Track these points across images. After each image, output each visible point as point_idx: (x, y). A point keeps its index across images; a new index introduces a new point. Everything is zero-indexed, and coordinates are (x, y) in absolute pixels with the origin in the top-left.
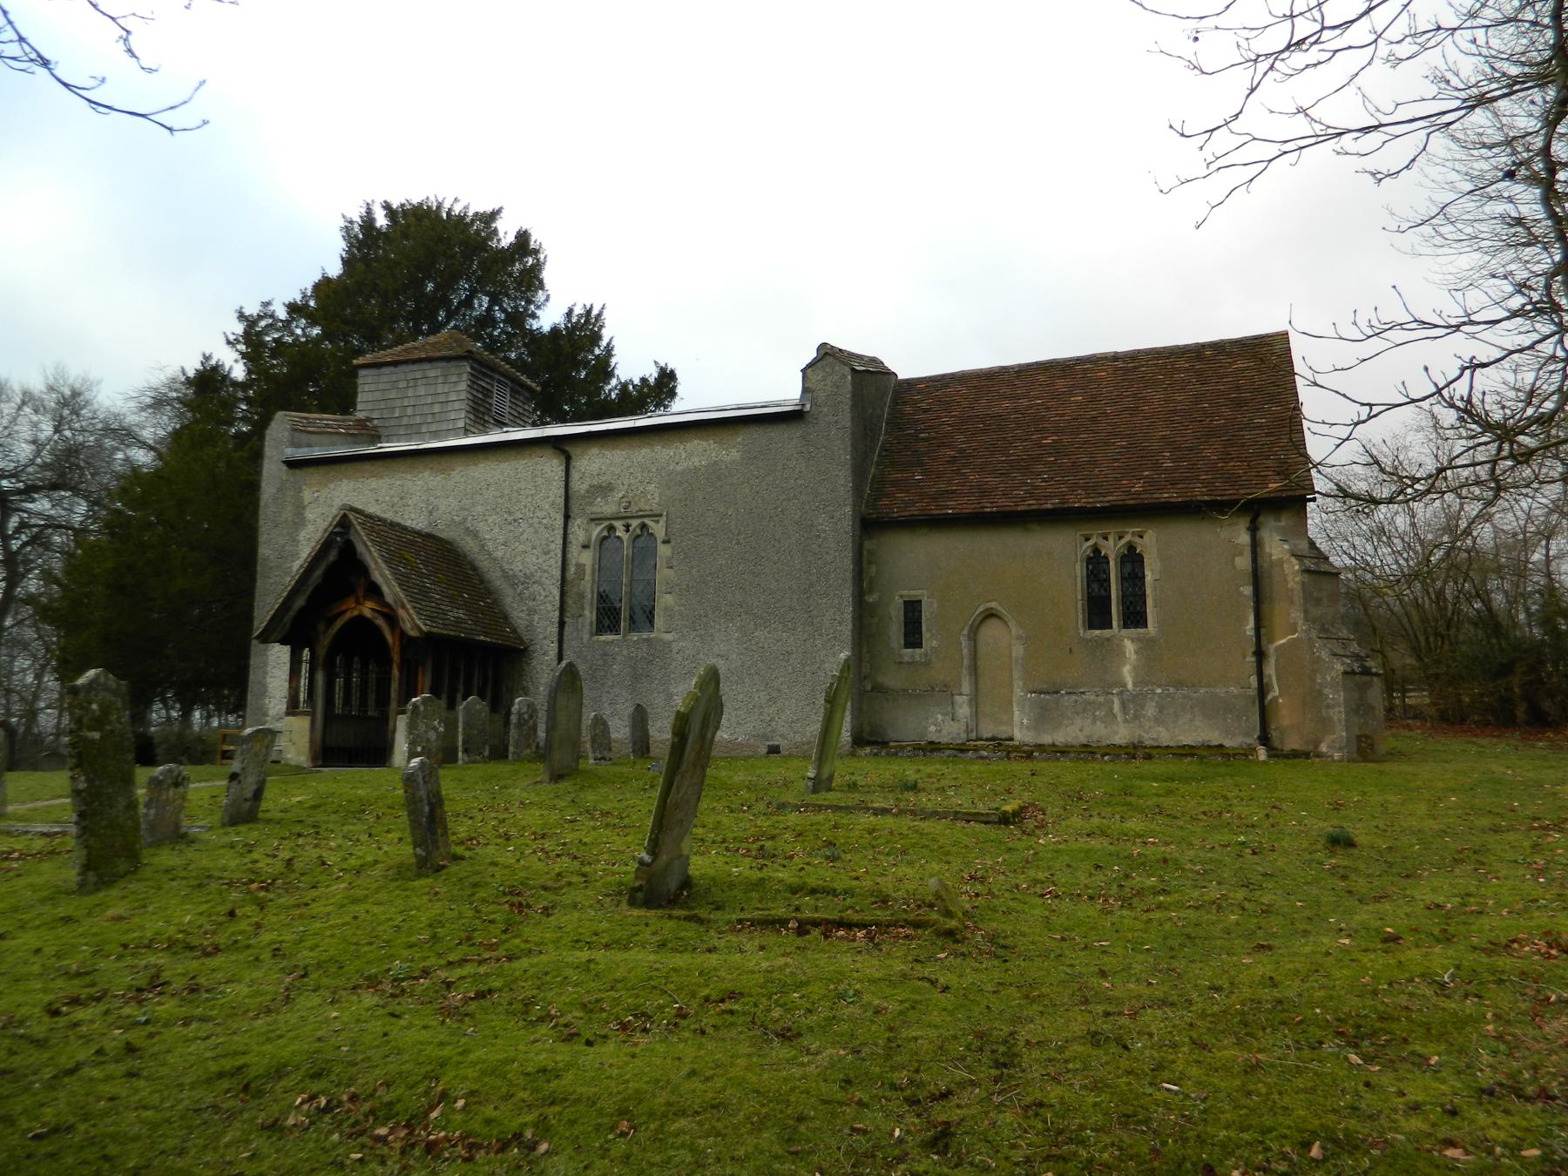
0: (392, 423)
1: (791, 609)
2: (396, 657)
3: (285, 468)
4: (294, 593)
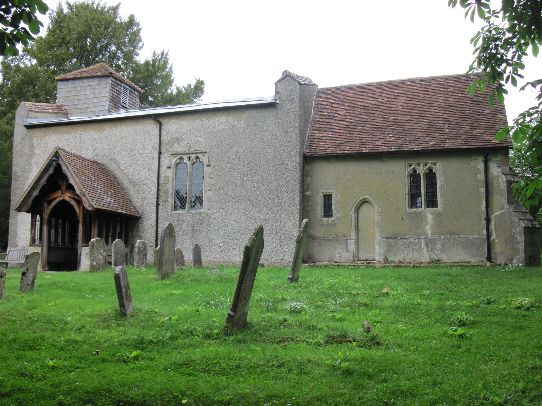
0: (73, 107)
1: (270, 198)
2: (81, 219)
3: (25, 128)
4: (33, 189)
